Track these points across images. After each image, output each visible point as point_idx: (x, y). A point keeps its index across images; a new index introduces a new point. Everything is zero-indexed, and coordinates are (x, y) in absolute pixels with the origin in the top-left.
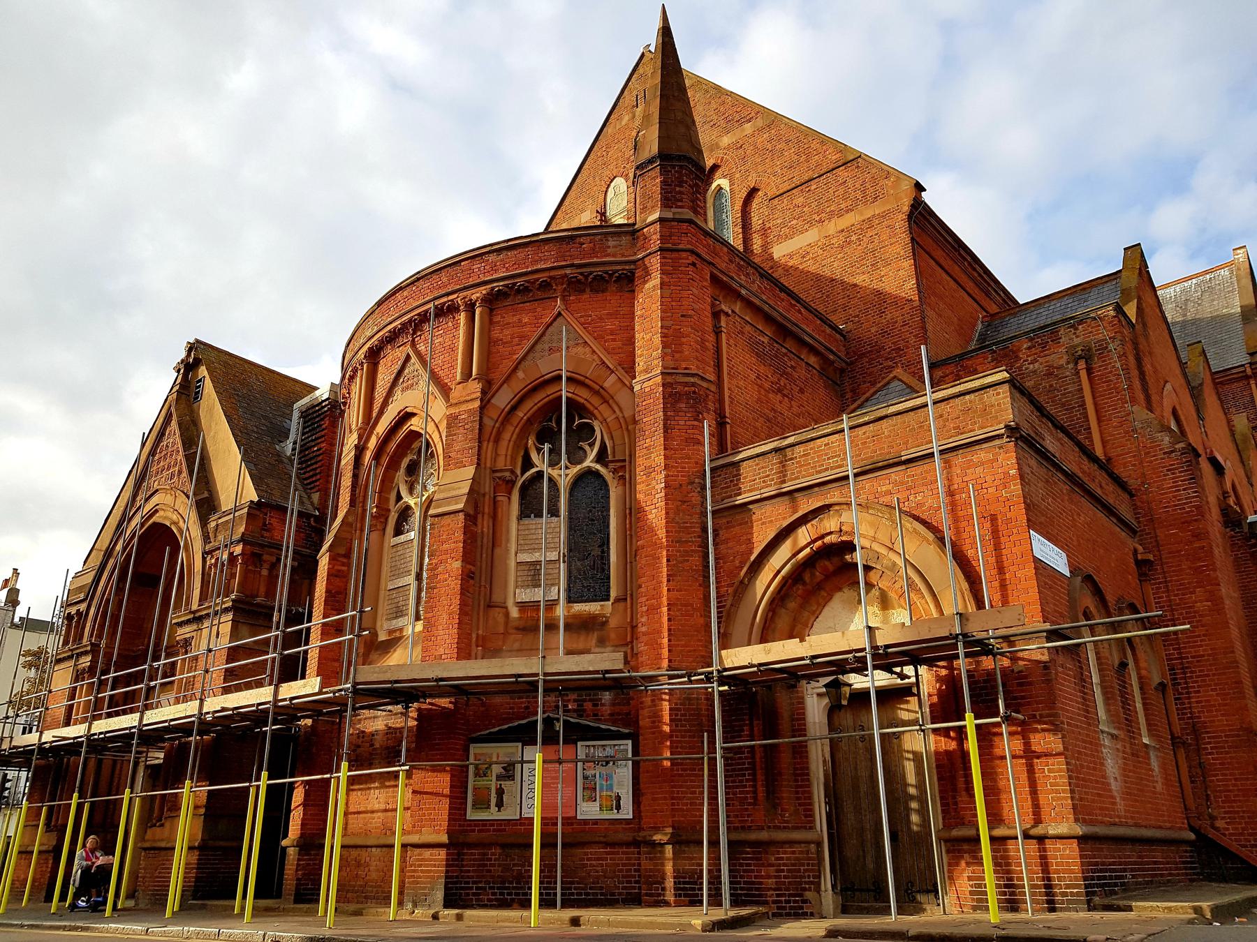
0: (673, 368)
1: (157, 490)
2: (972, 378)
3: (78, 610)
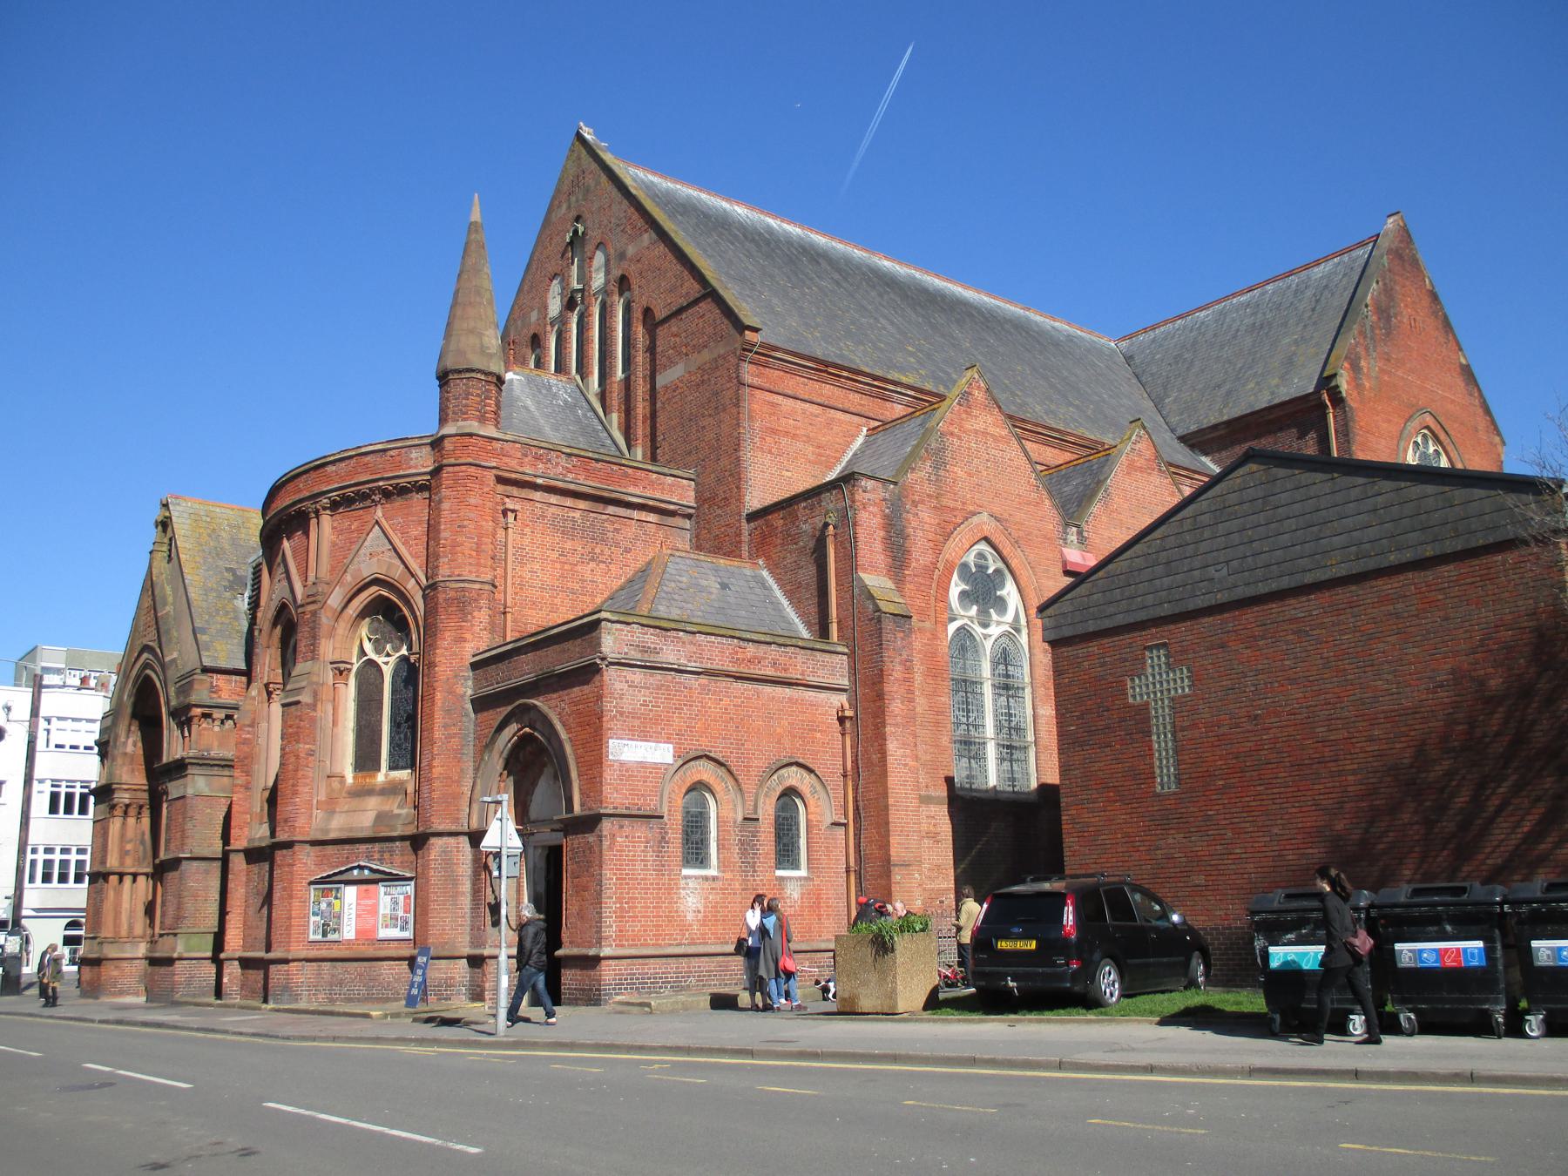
0: (449, 576)
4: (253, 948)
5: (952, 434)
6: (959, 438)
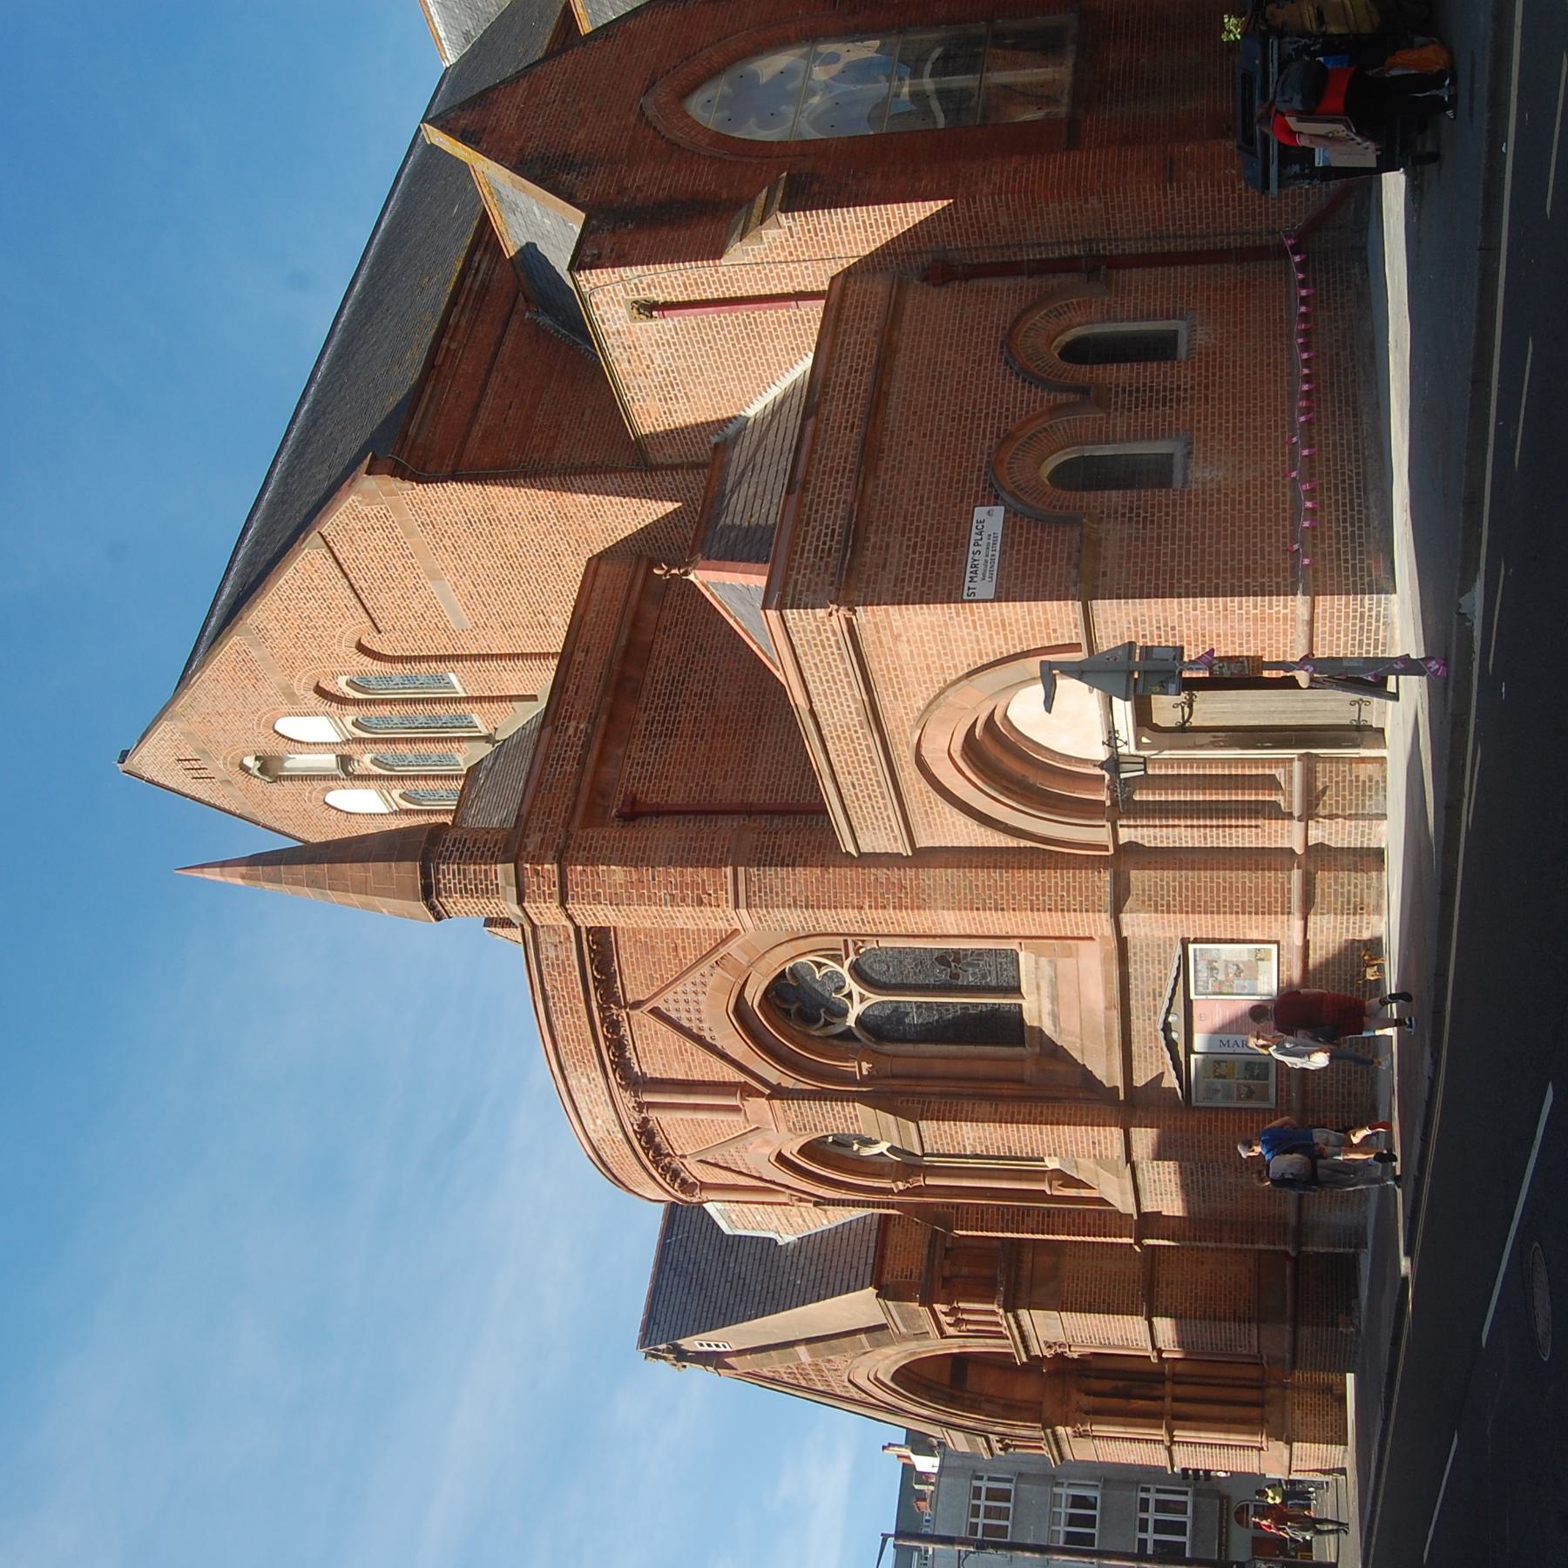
1: (850, 1381)
4: (1286, 891)
5: (521, 150)
6: (529, 139)
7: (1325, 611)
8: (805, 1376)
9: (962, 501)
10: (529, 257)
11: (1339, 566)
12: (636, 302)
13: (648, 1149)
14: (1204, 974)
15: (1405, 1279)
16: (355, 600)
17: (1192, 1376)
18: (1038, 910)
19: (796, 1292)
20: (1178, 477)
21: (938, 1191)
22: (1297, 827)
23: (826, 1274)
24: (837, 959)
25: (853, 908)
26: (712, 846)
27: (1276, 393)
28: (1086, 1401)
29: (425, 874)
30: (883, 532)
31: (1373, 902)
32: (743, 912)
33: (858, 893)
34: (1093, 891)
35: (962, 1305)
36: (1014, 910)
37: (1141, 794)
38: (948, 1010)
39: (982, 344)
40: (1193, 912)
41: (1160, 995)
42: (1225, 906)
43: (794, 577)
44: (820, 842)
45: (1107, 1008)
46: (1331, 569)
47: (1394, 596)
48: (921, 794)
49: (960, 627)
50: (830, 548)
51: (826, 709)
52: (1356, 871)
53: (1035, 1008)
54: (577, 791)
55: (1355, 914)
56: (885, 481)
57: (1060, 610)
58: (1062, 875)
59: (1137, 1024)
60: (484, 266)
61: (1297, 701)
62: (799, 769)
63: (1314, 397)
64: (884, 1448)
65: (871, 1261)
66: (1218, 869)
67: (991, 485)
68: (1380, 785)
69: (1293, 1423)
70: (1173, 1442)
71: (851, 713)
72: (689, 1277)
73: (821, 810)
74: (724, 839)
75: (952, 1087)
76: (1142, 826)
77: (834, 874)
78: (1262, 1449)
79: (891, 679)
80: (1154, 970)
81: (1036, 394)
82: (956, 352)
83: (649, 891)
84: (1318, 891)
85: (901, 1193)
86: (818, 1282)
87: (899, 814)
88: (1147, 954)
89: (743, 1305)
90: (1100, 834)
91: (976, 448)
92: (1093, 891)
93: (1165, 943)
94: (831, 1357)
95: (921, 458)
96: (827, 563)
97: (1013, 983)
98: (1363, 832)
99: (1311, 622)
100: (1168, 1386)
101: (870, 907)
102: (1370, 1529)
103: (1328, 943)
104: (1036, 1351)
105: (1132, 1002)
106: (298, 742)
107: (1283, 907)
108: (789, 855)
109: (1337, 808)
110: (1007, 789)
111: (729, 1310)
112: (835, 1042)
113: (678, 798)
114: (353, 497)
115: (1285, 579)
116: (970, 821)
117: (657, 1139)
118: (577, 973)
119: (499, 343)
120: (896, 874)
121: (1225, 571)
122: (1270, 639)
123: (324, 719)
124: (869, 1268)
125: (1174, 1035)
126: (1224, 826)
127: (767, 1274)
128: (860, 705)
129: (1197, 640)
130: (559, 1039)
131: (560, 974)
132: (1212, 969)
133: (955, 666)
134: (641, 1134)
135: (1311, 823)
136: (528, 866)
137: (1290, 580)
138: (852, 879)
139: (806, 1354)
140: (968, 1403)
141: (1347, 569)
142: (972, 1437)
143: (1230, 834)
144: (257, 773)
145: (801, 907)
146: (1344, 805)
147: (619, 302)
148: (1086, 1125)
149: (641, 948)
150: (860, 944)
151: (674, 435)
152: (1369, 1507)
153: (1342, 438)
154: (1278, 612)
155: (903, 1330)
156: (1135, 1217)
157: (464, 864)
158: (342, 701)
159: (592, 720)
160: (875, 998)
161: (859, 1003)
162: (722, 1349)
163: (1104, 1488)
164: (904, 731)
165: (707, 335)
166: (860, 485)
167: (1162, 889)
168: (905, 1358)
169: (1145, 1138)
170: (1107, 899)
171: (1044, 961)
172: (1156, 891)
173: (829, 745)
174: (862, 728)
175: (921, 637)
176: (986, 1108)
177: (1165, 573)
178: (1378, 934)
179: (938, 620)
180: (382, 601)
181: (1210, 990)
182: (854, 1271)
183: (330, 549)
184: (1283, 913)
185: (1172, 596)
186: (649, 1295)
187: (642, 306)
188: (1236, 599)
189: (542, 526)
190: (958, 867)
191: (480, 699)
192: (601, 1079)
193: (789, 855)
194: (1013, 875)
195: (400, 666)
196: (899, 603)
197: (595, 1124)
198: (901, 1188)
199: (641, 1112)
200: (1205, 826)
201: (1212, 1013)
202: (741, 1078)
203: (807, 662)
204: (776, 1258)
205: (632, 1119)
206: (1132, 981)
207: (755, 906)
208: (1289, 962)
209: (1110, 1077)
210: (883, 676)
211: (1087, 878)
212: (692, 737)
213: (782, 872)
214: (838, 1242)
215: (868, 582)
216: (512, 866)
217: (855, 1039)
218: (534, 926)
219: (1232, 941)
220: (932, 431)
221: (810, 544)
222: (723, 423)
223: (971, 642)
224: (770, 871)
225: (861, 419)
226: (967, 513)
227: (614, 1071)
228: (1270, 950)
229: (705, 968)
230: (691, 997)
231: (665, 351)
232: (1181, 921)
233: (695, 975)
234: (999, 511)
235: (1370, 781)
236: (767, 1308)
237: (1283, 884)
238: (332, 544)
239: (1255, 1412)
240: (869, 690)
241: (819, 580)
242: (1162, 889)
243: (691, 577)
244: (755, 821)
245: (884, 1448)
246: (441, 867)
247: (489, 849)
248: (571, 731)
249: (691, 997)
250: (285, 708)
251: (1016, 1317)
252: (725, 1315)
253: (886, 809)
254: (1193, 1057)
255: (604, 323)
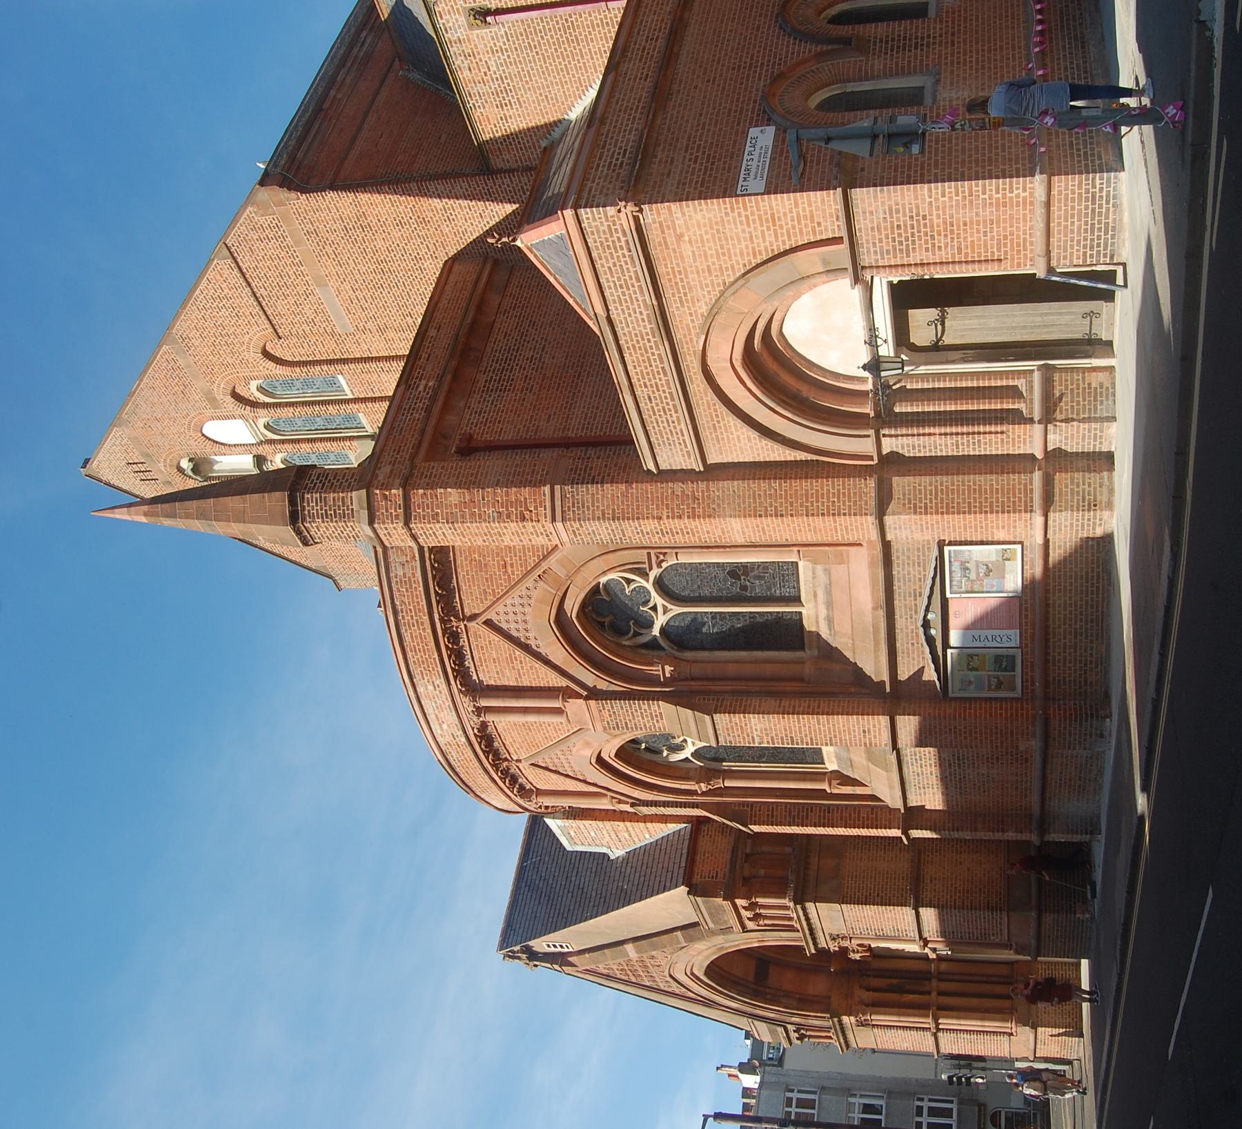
1: (671, 976)
2: (1113, 1063)
3: (797, 1039)
4: (1028, 492)
7: (1060, 193)
8: (634, 972)
9: (738, 124)
10: (398, 16)
11: (1072, 155)
12: (472, 9)
13: (488, 753)
14: (958, 575)
15: (1142, 818)
16: (258, 308)
17: (953, 974)
18: (813, 515)
19: (623, 895)
20: (928, 100)
21: (735, 792)
22: (1038, 429)
23: (647, 879)
24: (644, 575)
25: (653, 518)
26: (534, 470)
27: (1013, 36)
28: (867, 996)
29: (292, 502)
30: (669, 151)
31: (1105, 499)
32: (559, 525)
33: (657, 505)
34: (860, 497)
35: (761, 900)
36: (792, 515)
37: (901, 406)
38: (739, 619)
39: (760, 16)
40: (948, 513)
41: (920, 596)
42: (975, 507)
43: (589, 184)
44: (626, 464)
45: (875, 609)
46: (1065, 156)
47: (1122, 174)
48: (709, 408)
49: (735, 224)
50: (622, 163)
51: (622, 318)
52: (1090, 471)
53: (813, 615)
54: (423, 432)
55: (1089, 510)
56: (672, 115)
57: (823, 201)
58: (833, 483)
59: (900, 623)
60: (368, 41)
61: (1036, 315)
62: (611, 411)
63: (1047, 36)
64: (718, 1068)
65: (683, 865)
66: (969, 474)
67: (764, 112)
68: (1109, 392)
69: (1037, 1012)
70: (938, 1030)
71: (643, 320)
72: (539, 892)
73: (629, 442)
74: (544, 465)
75: (741, 686)
76: (902, 436)
77: (637, 489)
78: (1011, 1034)
79: (676, 283)
80: (915, 571)
81: (805, 47)
82: (738, 23)
83: (480, 510)
84: (1057, 490)
85: (704, 794)
86: (641, 885)
87: (690, 427)
88: (908, 557)
89: (581, 908)
90: (861, 445)
91: (752, 87)
92: (860, 497)
93: (923, 546)
94: (654, 953)
95: (705, 97)
96: (619, 174)
97: (793, 592)
98: (1095, 435)
99: (1048, 204)
100: (934, 983)
101: (668, 517)
102: (1105, 1086)
103: (1065, 543)
104: (823, 944)
105: (896, 602)
106: (222, 444)
107: (1026, 506)
108: (599, 475)
109: (1073, 413)
110: (784, 402)
111: (570, 915)
112: (643, 651)
113: (508, 436)
114: (250, 208)
115: (1023, 165)
116: (753, 434)
117: (496, 744)
118: (421, 589)
119: (377, 92)
120: (689, 487)
121: (970, 162)
122: (1011, 226)
123: (240, 422)
124: (682, 870)
125: (933, 632)
126: (974, 433)
127: (601, 883)
128: (650, 312)
129: (946, 230)
130: (408, 650)
131: (407, 591)
132: (965, 569)
133: (732, 267)
134: (481, 738)
135: (1050, 427)
136: (378, 492)
137: (1028, 166)
138: (652, 493)
139: (633, 951)
140: (769, 997)
141: (1079, 156)
142: (774, 1027)
143: (979, 441)
144: (191, 474)
145: (609, 519)
146: (1078, 410)
147: (458, 9)
148: (857, 714)
149: (476, 567)
150: (662, 557)
151: (511, 139)
152: (1104, 1065)
153: (1072, 63)
154: (1018, 196)
155: (711, 925)
156: (903, 811)
157: (325, 492)
158: (254, 404)
159: (440, 379)
160: (677, 610)
161: (663, 614)
162: (566, 950)
163: (887, 1098)
164: (691, 339)
165: (533, 41)
166: (650, 117)
167: (920, 493)
168: (715, 953)
169: (908, 725)
170: (873, 503)
171: (819, 568)
172: (915, 495)
173: (626, 355)
174: (654, 337)
175: (701, 236)
176: (772, 702)
177: (916, 166)
178: (1109, 531)
179: (715, 217)
180: (280, 308)
181: (963, 589)
182: (670, 874)
183: (234, 259)
184: (1026, 512)
185: (922, 182)
186: (508, 908)
187: (477, 12)
188: (980, 182)
189: (406, 232)
190: (743, 479)
191: (364, 400)
192: (444, 686)
193: (599, 475)
194: (791, 484)
195: (298, 370)
196: (681, 200)
197: (442, 729)
198: (704, 789)
199: (479, 716)
200: (957, 434)
201: (965, 610)
202: (563, 682)
203: (603, 266)
204: (608, 870)
205: (472, 722)
206: (896, 582)
207: (570, 519)
208: (1032, 561)
209: (877, 672)
210: (670, 280)
211: (855, 485)
212: (522, 391)
213: (592, 488)
214: (657, 852)
215: (654, 187)
216: (364, 492)
217: (660, 648)
218: (385, 548)
219: (982, 543)
220: (715, 78)
221: (605, 161)
222: (550, 126)
223: (745, 240)
224: (582, 488)
225: (653, 72)
226: (743, 132)
227: (455, 678)
228: (1015, 550)
229: (529, 582)
230: (518, 609)
231: (499, 57)
232: (937, 523)
233: (521, 590)
234: (771, 131)
235: (1101, 387)
236: (600, 910)
237: (1025, 485)
238: (236, 255)
239: (1006, 1003)
240: (658, 295)
241: (611, 186)
242: (920, 493)
243: (518, 243)
244: (572, 452)
245: (718, 1068)
246: (306, 496)
247: (347, 481)
248: (421, 388)
249: (518, 609)
250: (209, 412)
251: (804, 909)
252: (567, 918)
253: (679, 424)
254: (949, 651)
255: (447, 32)
